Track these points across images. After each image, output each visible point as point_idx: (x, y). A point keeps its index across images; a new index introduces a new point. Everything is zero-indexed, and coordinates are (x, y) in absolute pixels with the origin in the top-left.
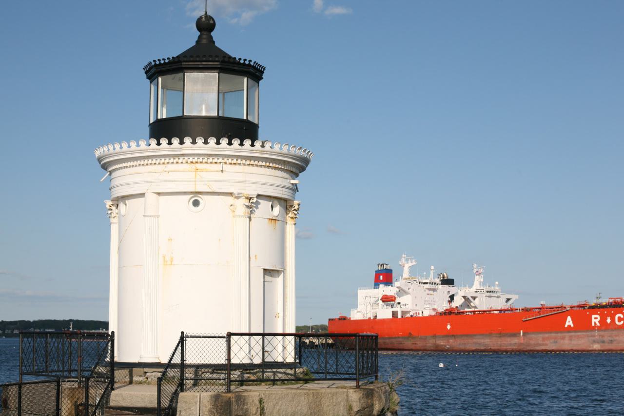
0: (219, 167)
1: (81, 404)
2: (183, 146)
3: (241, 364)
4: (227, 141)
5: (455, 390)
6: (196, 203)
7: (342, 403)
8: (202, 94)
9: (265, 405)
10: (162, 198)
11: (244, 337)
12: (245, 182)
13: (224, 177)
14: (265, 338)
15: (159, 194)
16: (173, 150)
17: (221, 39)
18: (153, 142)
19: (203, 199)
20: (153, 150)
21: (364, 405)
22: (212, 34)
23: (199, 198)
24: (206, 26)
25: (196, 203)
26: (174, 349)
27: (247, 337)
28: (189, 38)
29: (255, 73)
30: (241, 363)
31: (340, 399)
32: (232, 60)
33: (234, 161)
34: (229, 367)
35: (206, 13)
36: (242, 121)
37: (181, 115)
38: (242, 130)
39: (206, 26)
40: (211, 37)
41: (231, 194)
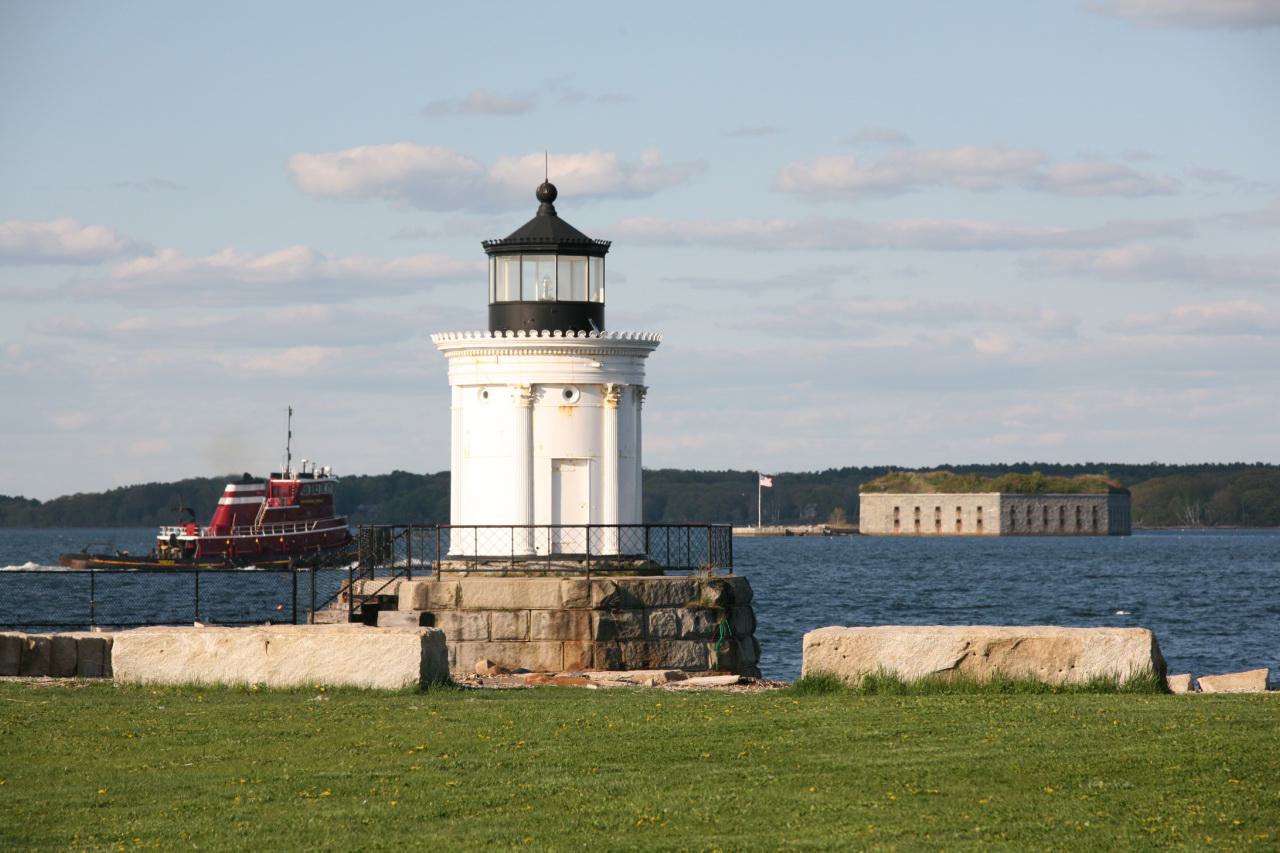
1: (467, 565)
2: (506, 339)
4: (549, 333)
6: (486, 395)
7: (553, 594)
8: (542, 279)
9: (463, 593)
10: (465, 389)
15: (462, 386)
16: (554, 342)
17: (564, 211)
18: (498, 334)
21: (575, 596)
22: (554, 203)
24: (548, 194)
25: (486, 395)
26: (926, 467)
28: (530, 211)
29: (596, 250)
31: (550, 590)
32: (587, 241)
35: (547, 181)
36: (584, 303)
38: (582, 316)
39: (548, 194)
40: (553, 208)
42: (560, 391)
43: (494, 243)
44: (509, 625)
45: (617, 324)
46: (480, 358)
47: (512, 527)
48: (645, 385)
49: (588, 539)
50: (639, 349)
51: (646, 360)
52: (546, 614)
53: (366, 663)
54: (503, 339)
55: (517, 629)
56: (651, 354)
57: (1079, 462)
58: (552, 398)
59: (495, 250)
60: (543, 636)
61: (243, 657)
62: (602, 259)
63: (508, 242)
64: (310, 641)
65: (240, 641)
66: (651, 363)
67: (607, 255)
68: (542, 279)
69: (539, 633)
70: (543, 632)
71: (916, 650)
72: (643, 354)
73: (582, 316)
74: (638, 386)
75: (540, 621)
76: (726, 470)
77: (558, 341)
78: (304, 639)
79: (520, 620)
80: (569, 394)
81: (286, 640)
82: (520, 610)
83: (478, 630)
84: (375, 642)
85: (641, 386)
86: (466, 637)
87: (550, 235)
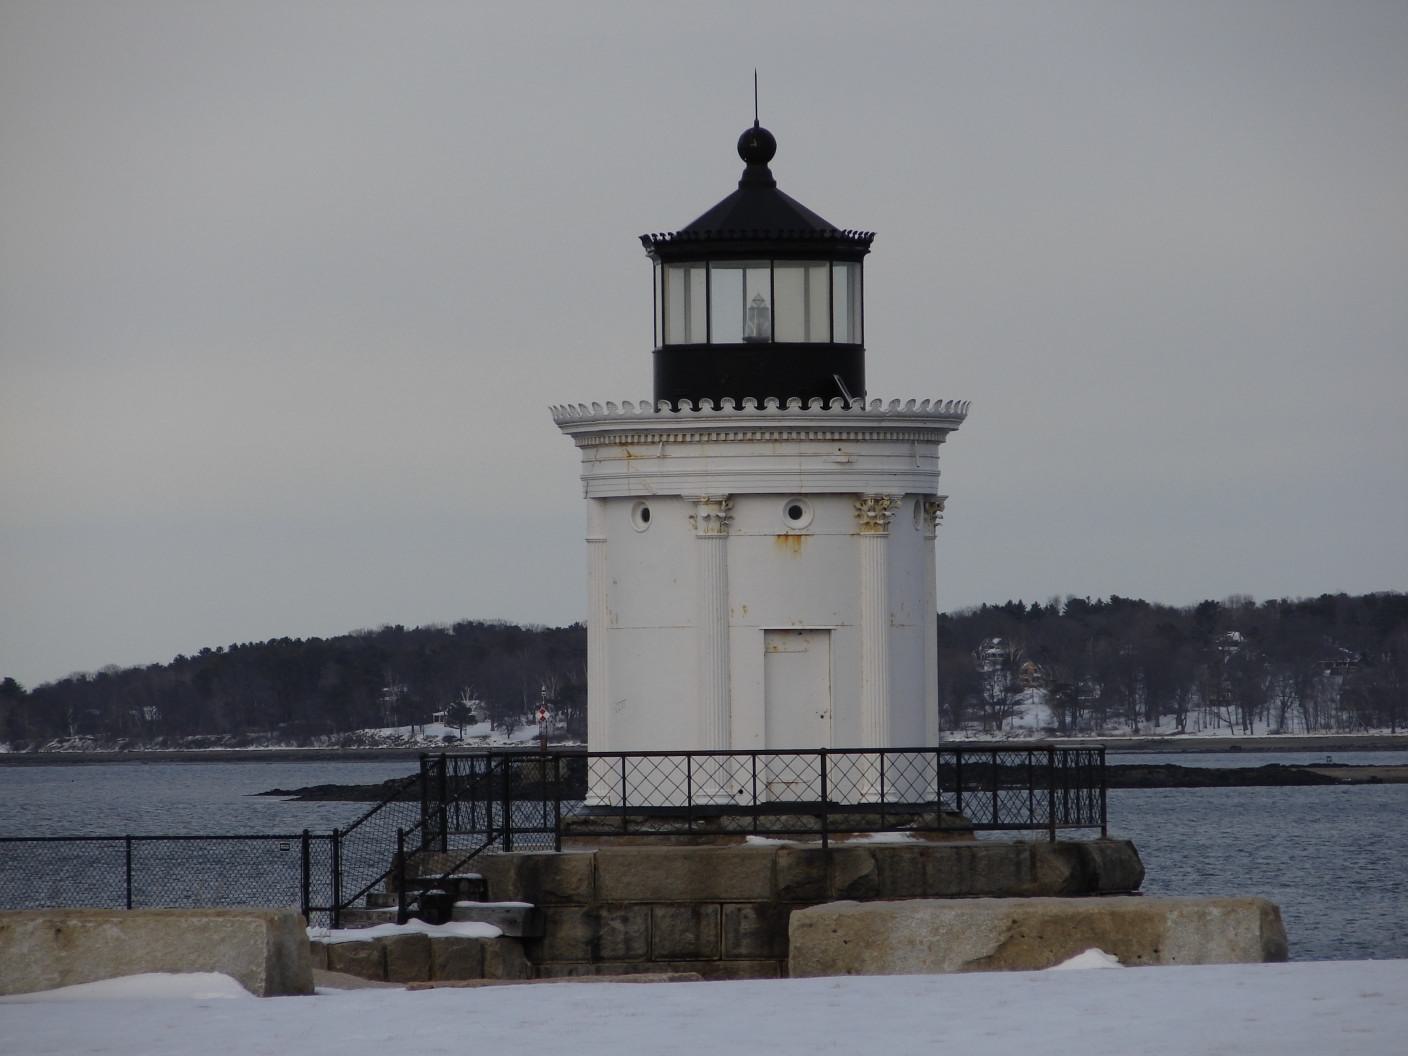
0: (656, 450)
3: (798, 803)
5: (1185, 857)
6: (646, 516)
8: (732, 304)
11: (606, 759)
12: (707, 474)
13: (670, 466)
14: (885, 758)
16: (764, 418)
17: (788, 175)
19: (654, 509)
20: (729, 418)
23: (653, 508)
24: (757, 147)
25: (646, 516)
27: (721, 759)
28: (727, 176)
30: (799, 800)
33: (776, 436)
34: (823, 808)
35: (757, 123)
37: (704, 341)
39: (757, 147)
41: (677, 497)
42: (780, 508)
43: (660, 238)
44: (684, 931)
45: (888, 381)
46: (634, 450)
47: (689, 754)
48: (940, 493)
49: (824, 775)
50: (927, 428)
51: (942, 446)
52: (748, 910)
53: (192, 957)
54: (780, 412)
55: (698, 937)
56: (950, 436)
57: (1206, 598)
58: (761, 521)
59: (670, 251)
60: (743, 951)
61: (25, 950)
62: (858, 266)
63: (685, 237)
64: (115, 930)
65: (20, 929)
66: (952, 450)
67: (867, 258)
68: (732, 304)
69: (737, 945)
70: (745, 942)
71: (942, 931)
72: (933, 438)
73: (826, 371)
74: (926, 496)
75: (739, 923)
76: (554, 627)
77: (815, 417)
78: (107, 926)
79: (704, 923)
80: (795, 513)
81: (84, 926)
82: (704, 903)
83: (628, 941)
84: (204, 929)
85: (933, 495)
86: (605, 953)
87: (758, 223)
